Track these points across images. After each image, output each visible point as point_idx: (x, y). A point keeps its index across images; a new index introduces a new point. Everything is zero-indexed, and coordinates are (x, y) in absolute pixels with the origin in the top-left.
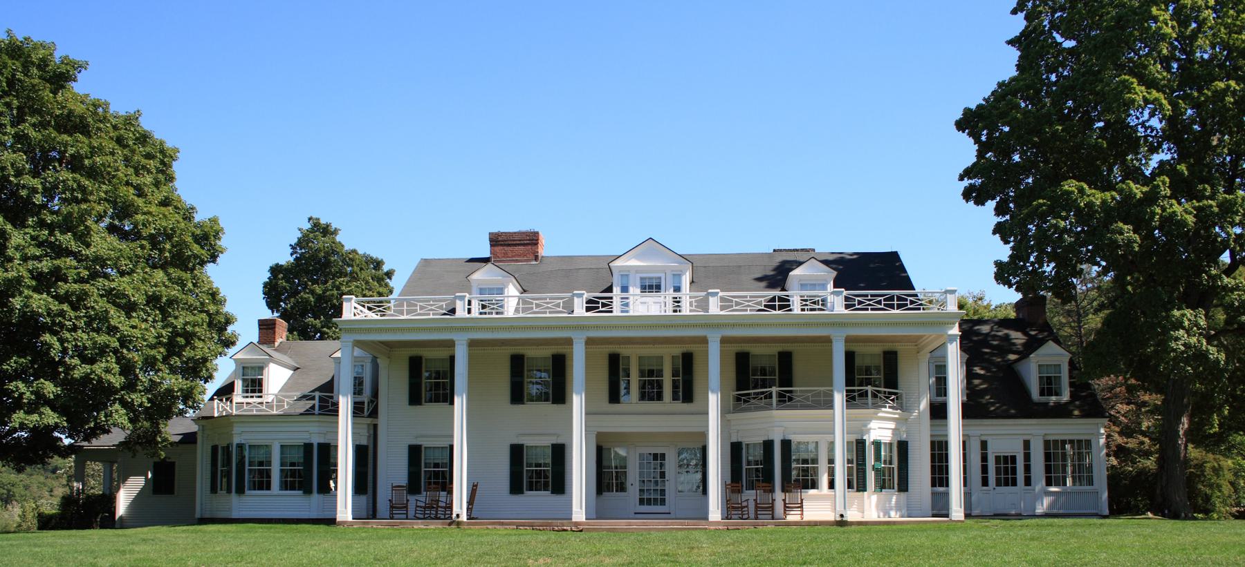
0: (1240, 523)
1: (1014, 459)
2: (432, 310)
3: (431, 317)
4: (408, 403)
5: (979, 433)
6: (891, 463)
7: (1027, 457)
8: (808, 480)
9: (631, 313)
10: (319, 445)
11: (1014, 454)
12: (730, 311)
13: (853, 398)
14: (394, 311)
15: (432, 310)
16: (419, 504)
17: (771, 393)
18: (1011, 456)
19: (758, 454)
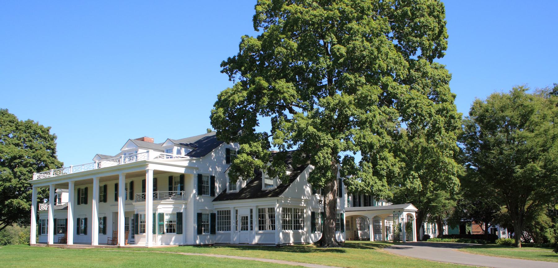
0: (303, 255)
1: (247, 217)
5: (233, 206)
6: (208, 223)
7: (251, 216)
16: (109, 239)
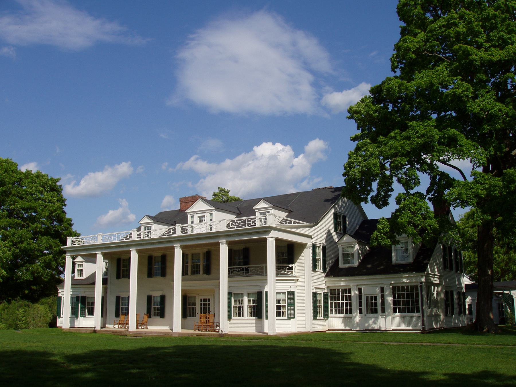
2: (236, 225)
3: (236, 229)
4: (147, 276)
8: (416, 307)
9: (152, 238)
10: (82, 297)
11: (376, 295)
12: (184, 233)
13: (232, 272)
14: (242, 225)
15: (236, 225)
17: (263, 267)
18: (374, 296)
19: (158, 300)
